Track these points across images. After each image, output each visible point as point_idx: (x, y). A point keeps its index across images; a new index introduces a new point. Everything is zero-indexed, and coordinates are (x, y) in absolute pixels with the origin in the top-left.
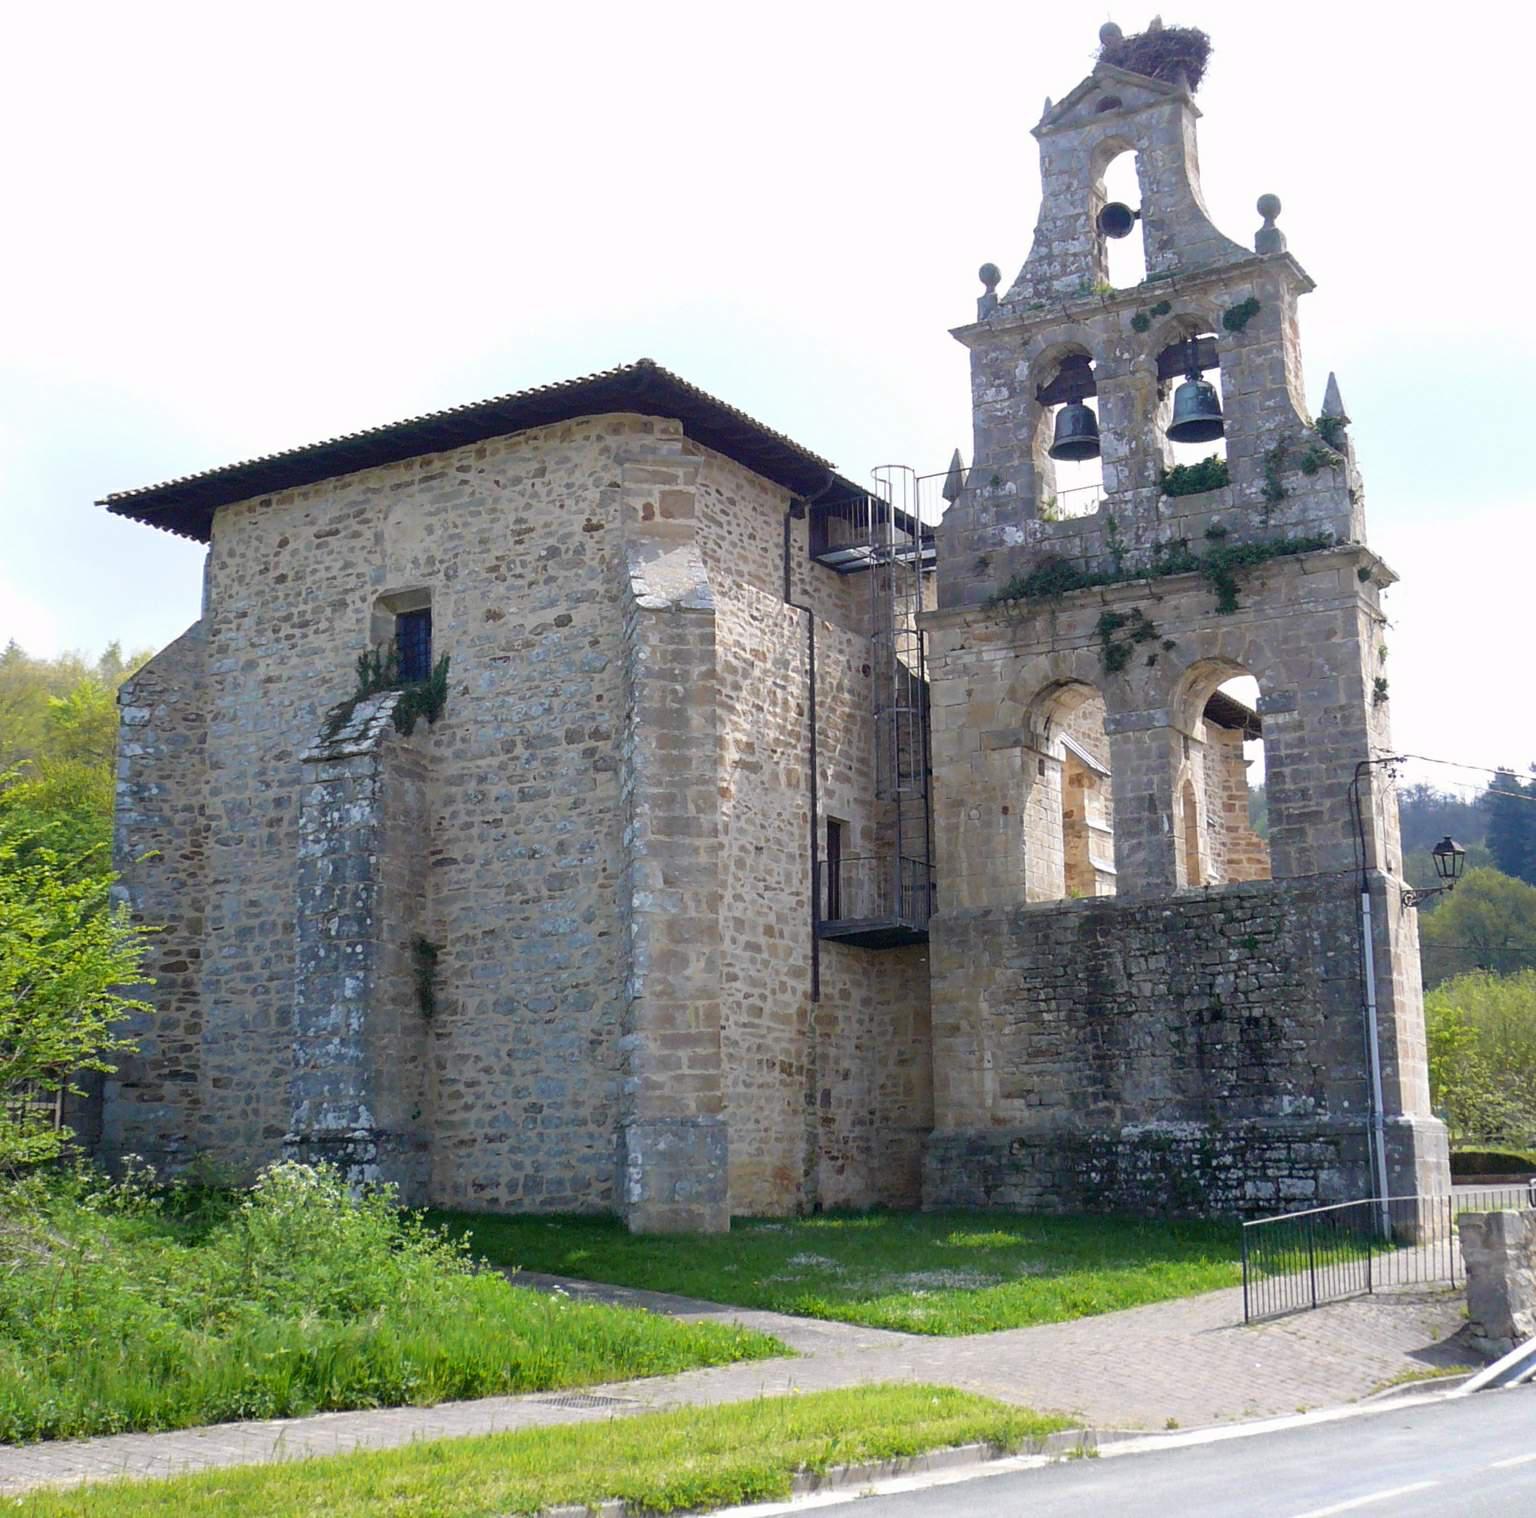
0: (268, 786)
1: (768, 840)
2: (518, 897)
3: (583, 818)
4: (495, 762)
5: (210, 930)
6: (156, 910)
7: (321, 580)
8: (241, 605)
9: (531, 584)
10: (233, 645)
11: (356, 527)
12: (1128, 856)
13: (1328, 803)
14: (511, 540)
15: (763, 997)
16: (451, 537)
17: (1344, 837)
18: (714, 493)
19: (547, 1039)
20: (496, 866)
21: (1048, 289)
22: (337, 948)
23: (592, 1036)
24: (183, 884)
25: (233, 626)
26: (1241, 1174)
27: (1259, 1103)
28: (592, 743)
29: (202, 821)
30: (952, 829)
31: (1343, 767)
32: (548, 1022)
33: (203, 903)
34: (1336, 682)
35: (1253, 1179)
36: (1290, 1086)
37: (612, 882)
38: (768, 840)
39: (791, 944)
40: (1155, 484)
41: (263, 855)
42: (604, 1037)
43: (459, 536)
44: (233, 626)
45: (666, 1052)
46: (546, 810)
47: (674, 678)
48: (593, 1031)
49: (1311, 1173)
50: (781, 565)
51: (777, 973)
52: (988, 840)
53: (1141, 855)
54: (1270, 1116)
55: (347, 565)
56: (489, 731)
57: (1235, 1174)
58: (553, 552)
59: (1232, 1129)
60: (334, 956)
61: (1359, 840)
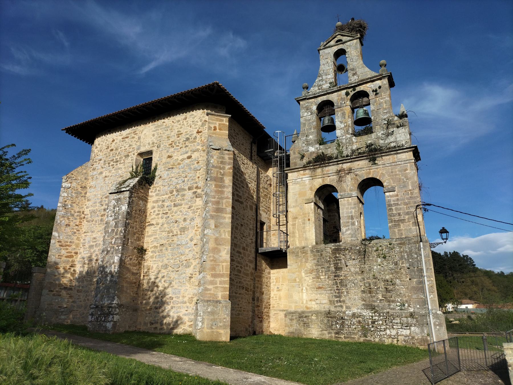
0: (102, 205)
1: (244, 223)
2: (171, 234)
3: (192, 211)
4: (167, 196)
5: (82, 246)
6: (66, 240)
7: (122, 150)
8: (100, 158)
9: (181, 148)
10: (97, 168)
11: (133, 136)
12: (345, 232)
13: (407, 217)
14: (176, 137)
15: (241, 267)
16: (159, 137)
17: (412, 226)
18: (233, 130)
19: (176, 277)
20: (165, 225)
21: (321, 88)
22: (113, 247)
23: (190, 276)
24: (75, 233)
25: (98, 163)
26: (385, 327)
27: (389, 305)
28: (195, 190)
29: (83, 216)
30: (294, 225)
31: (411, 207)
32: (178, 271)
33: (81, 238)
34: (408, 183)
35: (389, 329)
36: (399, 300)
37: (199, 229)
38: (244, 223)
39: (250, 253)
40: (351, 134)
41: (99, 224)
42: (194, 276)
43: (162, 136)
44: (98, 163)
45: (212, 279)
46: (181, 209)
47: (221, 169)
48: (190, 274)
49: (408, 328)
50: (250, 154)
51: (246, 261)
52: (304, 228)
53: (349, 232)
54: (394, 309)
55: (130, 146)
56: (166, 188)
57: (383, 327)
58: (188, 139)
59: (381, 313)
60: (112, 250)
61: (418, 227)
